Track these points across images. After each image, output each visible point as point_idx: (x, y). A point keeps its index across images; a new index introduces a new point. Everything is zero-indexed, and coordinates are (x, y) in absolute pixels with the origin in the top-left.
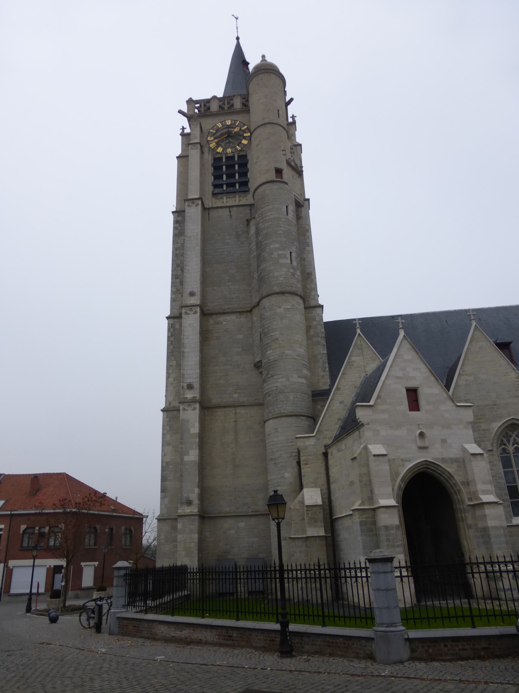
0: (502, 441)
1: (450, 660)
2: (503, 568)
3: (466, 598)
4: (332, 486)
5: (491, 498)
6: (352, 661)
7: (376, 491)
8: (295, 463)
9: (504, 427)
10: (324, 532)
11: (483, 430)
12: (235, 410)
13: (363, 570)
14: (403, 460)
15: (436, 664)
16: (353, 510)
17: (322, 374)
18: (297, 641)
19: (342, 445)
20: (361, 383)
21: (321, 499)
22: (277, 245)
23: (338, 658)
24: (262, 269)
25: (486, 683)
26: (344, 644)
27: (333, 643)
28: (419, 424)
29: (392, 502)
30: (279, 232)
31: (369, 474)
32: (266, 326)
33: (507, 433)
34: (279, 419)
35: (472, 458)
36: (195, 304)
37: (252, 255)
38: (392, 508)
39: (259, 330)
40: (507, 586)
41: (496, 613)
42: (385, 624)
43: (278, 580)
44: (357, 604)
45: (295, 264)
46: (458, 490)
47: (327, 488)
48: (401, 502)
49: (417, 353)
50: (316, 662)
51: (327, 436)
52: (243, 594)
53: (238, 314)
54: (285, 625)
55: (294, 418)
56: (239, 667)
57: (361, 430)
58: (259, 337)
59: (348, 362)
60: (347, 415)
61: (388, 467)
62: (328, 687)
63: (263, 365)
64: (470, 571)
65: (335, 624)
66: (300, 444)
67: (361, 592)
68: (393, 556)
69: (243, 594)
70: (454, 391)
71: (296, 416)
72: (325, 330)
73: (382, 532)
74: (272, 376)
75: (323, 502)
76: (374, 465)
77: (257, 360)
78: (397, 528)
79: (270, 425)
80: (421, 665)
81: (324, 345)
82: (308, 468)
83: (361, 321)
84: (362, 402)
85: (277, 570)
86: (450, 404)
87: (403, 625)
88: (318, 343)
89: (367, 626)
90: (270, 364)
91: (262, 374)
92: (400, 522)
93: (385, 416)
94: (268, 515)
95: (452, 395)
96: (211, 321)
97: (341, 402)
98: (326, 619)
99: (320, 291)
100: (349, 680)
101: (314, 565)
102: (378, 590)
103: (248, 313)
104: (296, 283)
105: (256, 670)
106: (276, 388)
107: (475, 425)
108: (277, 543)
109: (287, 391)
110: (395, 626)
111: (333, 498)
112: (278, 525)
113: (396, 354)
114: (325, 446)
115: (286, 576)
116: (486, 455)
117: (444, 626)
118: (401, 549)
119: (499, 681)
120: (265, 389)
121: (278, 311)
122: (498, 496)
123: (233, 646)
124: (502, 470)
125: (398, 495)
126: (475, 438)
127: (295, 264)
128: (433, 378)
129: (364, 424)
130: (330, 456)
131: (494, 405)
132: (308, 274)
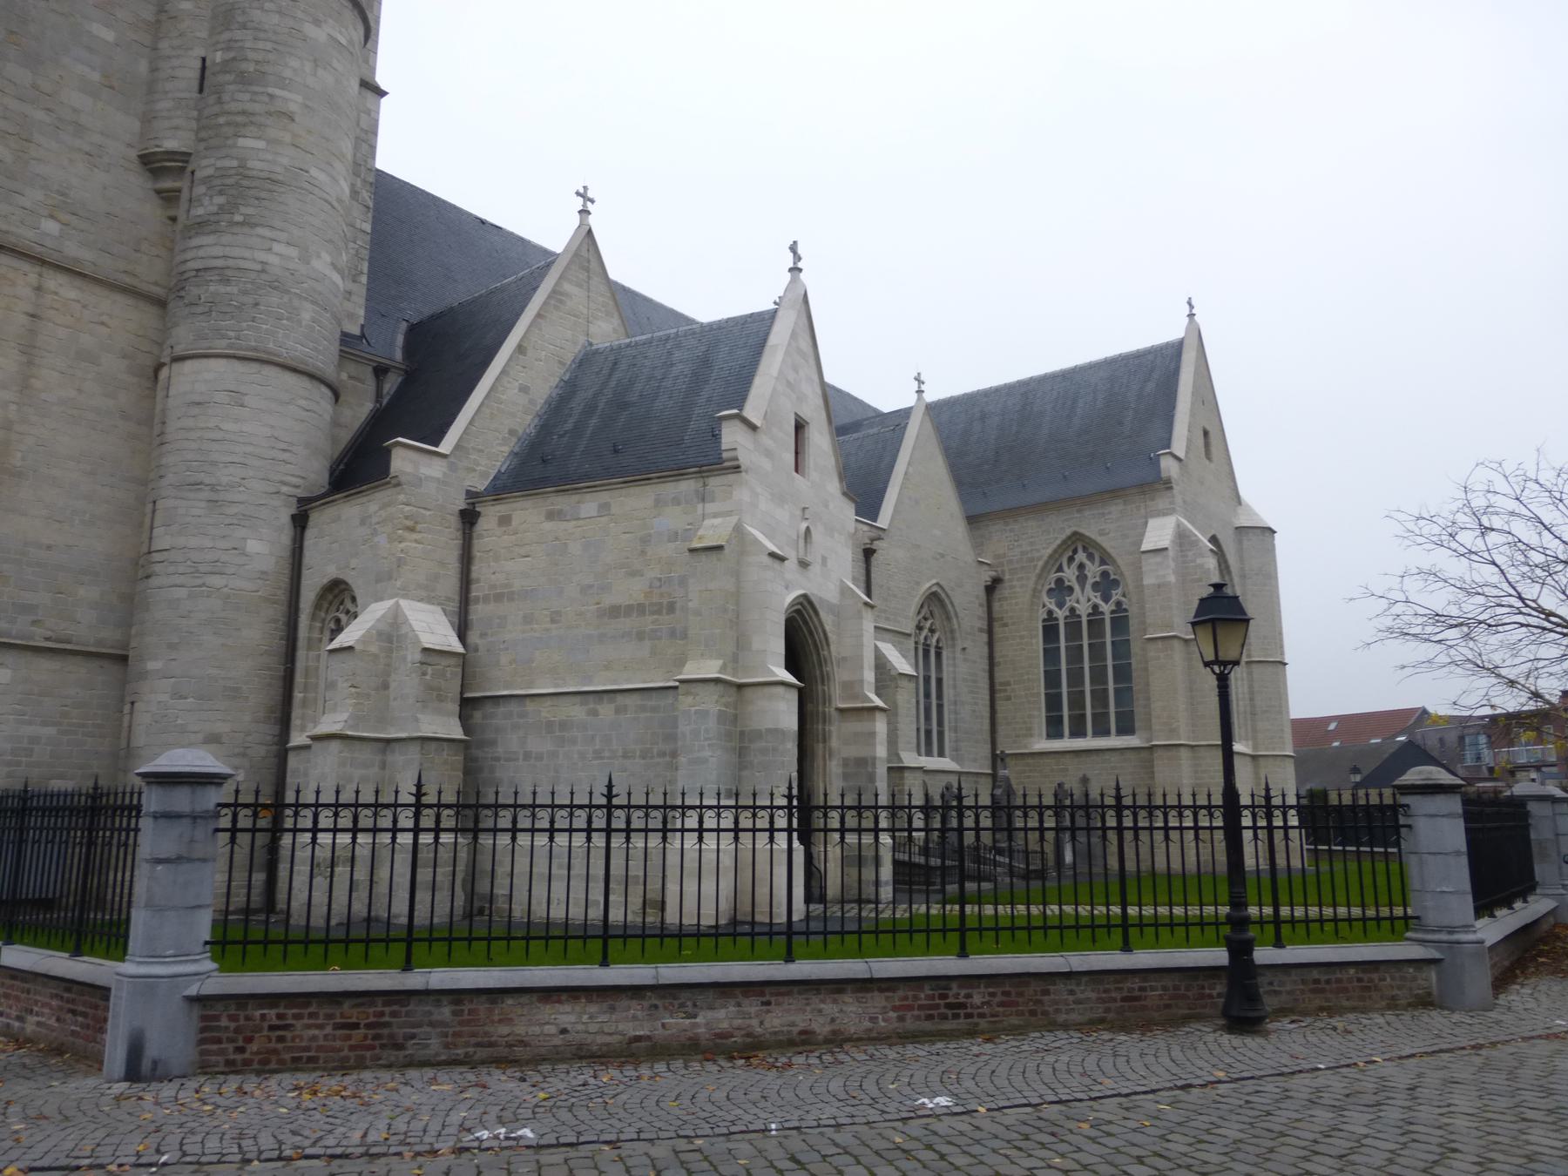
10: (460, 730)
12: (40, 275)
13: (1187, 813)
27: (1328, 982)
34: (255, 367)
47: (457, 610)
55: (305, 382)
71: (312, 376)
74: (248, 223)
81: (368, 207)
90: (245, 183)
97: (524, 389)
98: (1133, 932)
106: (259, 267)
121: (310, 30)
129: (743, 468)
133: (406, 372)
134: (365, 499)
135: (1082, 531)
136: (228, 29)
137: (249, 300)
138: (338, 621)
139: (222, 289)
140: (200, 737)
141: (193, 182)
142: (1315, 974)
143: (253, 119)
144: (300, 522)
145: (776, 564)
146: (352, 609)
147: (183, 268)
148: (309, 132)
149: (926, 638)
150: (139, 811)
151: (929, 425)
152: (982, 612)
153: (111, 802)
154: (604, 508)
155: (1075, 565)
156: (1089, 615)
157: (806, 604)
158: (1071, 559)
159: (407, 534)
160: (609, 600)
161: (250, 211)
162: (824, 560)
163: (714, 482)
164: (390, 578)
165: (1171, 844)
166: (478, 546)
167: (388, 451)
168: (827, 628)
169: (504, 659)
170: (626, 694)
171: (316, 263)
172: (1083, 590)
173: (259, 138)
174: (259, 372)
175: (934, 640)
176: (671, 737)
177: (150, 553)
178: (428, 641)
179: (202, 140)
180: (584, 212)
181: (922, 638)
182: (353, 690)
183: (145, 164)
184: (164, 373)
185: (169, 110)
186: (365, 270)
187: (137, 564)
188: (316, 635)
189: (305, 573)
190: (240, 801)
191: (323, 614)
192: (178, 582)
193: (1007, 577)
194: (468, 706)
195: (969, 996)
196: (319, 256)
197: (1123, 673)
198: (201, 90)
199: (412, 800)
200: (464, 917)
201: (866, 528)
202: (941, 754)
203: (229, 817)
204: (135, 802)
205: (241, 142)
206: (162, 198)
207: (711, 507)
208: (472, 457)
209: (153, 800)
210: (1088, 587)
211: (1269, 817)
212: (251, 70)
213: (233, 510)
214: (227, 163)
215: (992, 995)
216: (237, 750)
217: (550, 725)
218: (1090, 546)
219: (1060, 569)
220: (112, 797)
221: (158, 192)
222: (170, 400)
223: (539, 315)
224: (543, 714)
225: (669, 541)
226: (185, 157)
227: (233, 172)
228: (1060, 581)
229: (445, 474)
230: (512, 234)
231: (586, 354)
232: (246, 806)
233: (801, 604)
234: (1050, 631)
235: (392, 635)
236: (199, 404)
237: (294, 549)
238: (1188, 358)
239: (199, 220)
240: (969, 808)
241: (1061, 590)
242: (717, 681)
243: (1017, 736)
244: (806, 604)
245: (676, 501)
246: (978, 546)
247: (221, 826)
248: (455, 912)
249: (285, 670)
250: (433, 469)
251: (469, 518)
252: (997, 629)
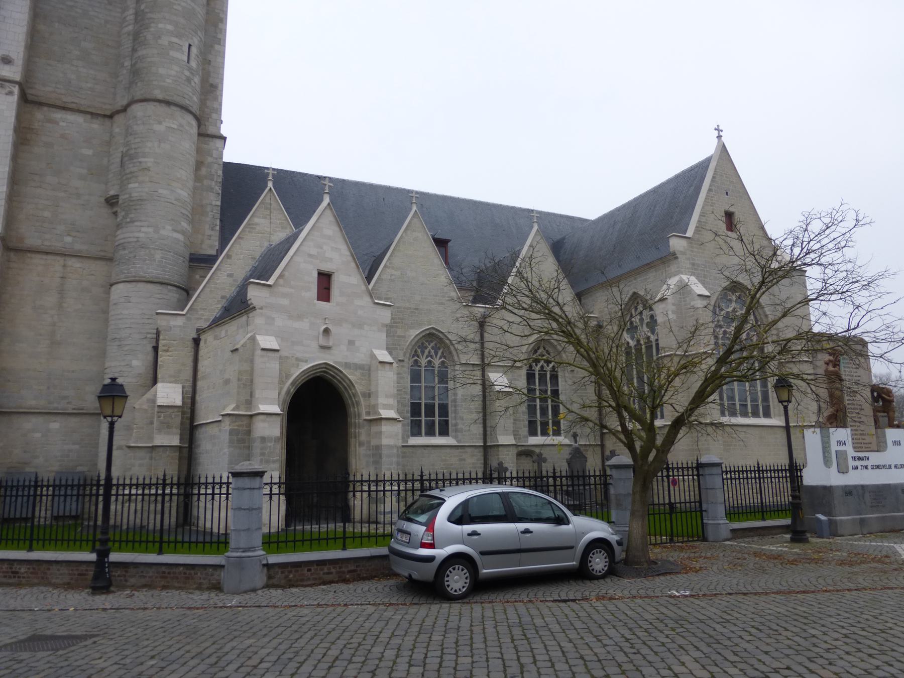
0: (416, 351)
1: (311, 586)
2: (373, 488)
3: (342, 522)
4: (200, 384)
5: (392, 414)
6: (190, 593)
7: (258, 394)
8: (149, 348)
9: (421, 335)
11: (398, 336)
14: (298, 359)
15: (294, 590)
16: (223, 415)
17: (208, 232)
18: (119, 573)
19: (222, 331)
21: (181, 399)
22: (170, 27)
23: (173, 591)
24: (139, 57)
25: (345, 605)
26: (185, 573)
27: (169, 573)
29: (276, 409)
30: (175, 7)
31: (251, 373)
32: (133, 146)
33: (423, 344)
34: (134, 284)
35: (379, 366)
36: (11, 79)
37: (126, 30)
38: (274, 416)
39: (121, 149)
40: (388, 509)
43: (101, 498)
44: (208, 530)
45: (193, 64)
46: (356, 402)
48: (286, 409)
49: (341, 230)
50: (142, 597)
52: (42, 520)
53: (89, 116)
54: (103, 554)
55: (158, 287)
56: (23, 610)
57: (251, 315)
58: (119, 160)
59: (248, 224)
60: (235, 294)
61: (277, 366)
62: (154, 623)
63: (120, 202)
65: (175, 551)
66: (162, 322)
67: (216, 514)
68: (265, 470)
69: (42, 520)
70: (374, 286)
71: (161, 283)
72: (223, 173)
73: (257, 445)
74: (132, 222)
75: (183, 402)
76: (260, 360)
77: (112, 193)
78: (277, 440)
79: (119, 290)
80: (277, 593)
82: (169, 356)
83: (275, 172)
84: (258, 279)
85: (102, 485)
86: (367, 299)
87: (263, 550)
88: (210, 189)
89: (218, 552)
90: (131, 204)
91: (116, 215)
92: (282, 433)
93: (285, 302)
94: (98, 414)
95: (372, 290)
96: (39, 115)
97: (230, 275)
99: (224, 116)
100: (184, 614)
101: (158, 479)
102: (240, 509)
103: (106, 119)
104: (190, 94)
105: (52, 612)
106: (135, 240)
107: (390, 329)
108: (106, 448)
110: (253, 551)
111: (198, 398)
112: (112, 425)
113: (314, 225)
114: (198, 330)
115: (114, 492)
116: (395, 365)
117: (311, 549)
118: (277, 465)
119: (359, 603)
120: (117, 238)
121: (157, 127)
122: (399, 412)
123: (19, 585)
124: (409, 384)
125: (284, 402)
126: (387, 344)
127: (193, 64)
128: (353, 265)
130: (202, 344)
131: (417, 309)
132: (212, 85)
137: (132, 255)
142: (163, 569)
148: (158, 174)
165: (215, 502)
171: (163, 232)
180: (719, 137)
195: (20, 569)
196: (164, 228)
208: (200, 313)
210: (644, 326)
213: (126, 348)
215: (29, 569)
229: (184, 323)
230: (337, 179)
248: (130, 523)
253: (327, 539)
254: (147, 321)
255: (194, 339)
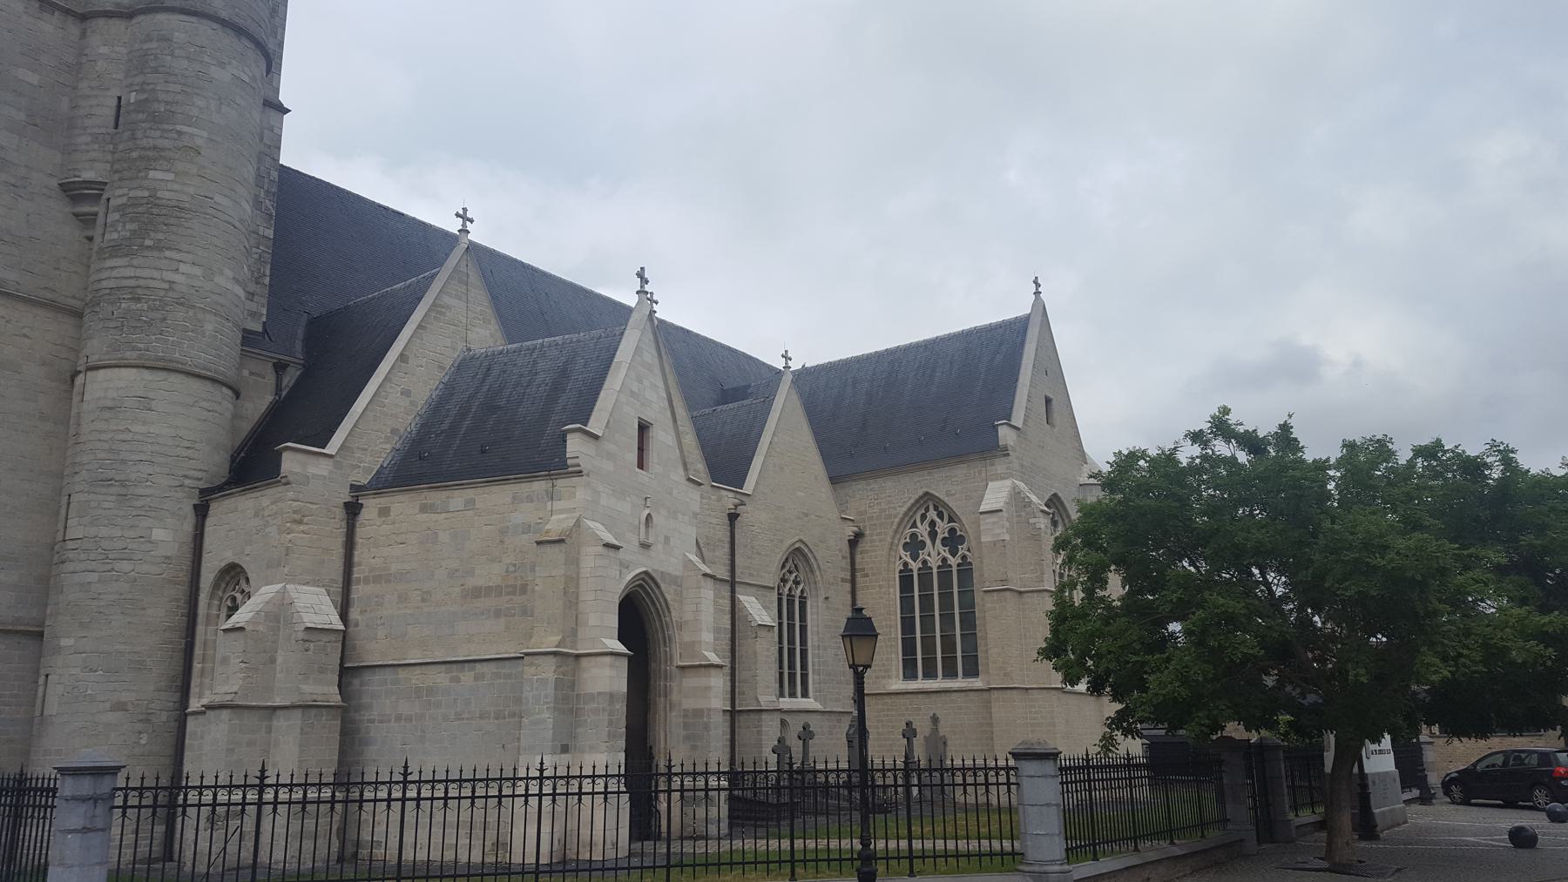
20: (454, 362)
28: (646, 498)
34: (162, 375)
41: (926, 854)
42: (1058, 860)
51: (362, 465)
55: (208, 386)
64: (916, 782)
71: (213, 380)
74: (158, 246)
81: (271, 215)
90: (155, 211)
97: (406, 393)
106: (166, 286)
109: (202, 306)
121: (215, 72)
133: (304, 366)
134: (259, 493)
135: (931, 491)
136: (142, 73)
137: (158, 315)
138: (234, 599)
139: (134, 306)
140: (108, 705)
141: (108, 208)
143: (163, 154)
144: (202, 511)
145: (611, 553)
146: (247, 590)
147: (97, 286)
149: (790, 589)
150: (54, 793)
151: (795, 397)
152: (846, 564)
153: (33, 785)
154: (470, 503)
155: (926, 522)
156: (939, 567)
157: (646, 578)
158: (923, 517)
159: (294, 526)
160: (472, 582)
161: (160, 236)
162: (667, 539)
163: (561, 483)
164: (279, 565)
166: (361, 533)
167: (279, 454)
168: (668, 597)
169: (381, 633)
170: (485, 664)
171: (218, 279)
172: (934, 544)
173: (168, 171)
174: (166, 380)
175: (798, 592)
176: (518, 700)
177: (65, 541)
178: (311, 620)
179: (116, 172)
181: (786, 591)
182: (244, 665)
183: (65, 191)
184: (79, 380)
185: (87, 144)
186: (268, 272)
187: (53, 548)
188: (214, 612)
189: (205, 557)
190: (130, 786)
191: (220, 593)
192: (90, 568)
193: (868, 532)
194: (347, 674)
196: (221, 273)
197: (969, 620)
198: (116, 127)
199: (257, 781)
200: (338, 861)
201: (731, 495)
202: (805, 694)
203: (122, 798)
204: (52, 786)
205: (152, 174)
206: (80, 220)
207: (557, 505)
208: (357, 455)
209: (67, 787)
210: (938, 542)
211: (907, 777)
212: (163, 110)
213: (139, 503)
214: (139, 193)
216: (141, 717)
217: (418, 690)
218: (941, 508)
219: (914, 525)
220: (34, 781)
221: (76, 215)
222: (85, 406)
223: (420, 326)
224: (414, 681)
225: (523, 533)
226: (101, 185)
227: (144, 201)
228: (914, 536)
229: (330, 472)
230: (414, 219)
231: (464, 359)
232: (134, 789)
233: (643, 579)
234: (906, 580)
235: (280, 613)
236: (110, 408)
237: (196, 535)
238: (1033, 334)
239: (113, 244)
240: (676, 774)
241: (914, 546)
242: (555, 654)
243: (877, 678)
244: (646, 578)
245: (530, 499)
246: (842, 505)
247: (116, 804)
249: (186, 644)
250: (320, 468)
251: (352, 510)
252: (859, 579)
253: (817, 860)
254: (185, 453)
255: (346, 505)
